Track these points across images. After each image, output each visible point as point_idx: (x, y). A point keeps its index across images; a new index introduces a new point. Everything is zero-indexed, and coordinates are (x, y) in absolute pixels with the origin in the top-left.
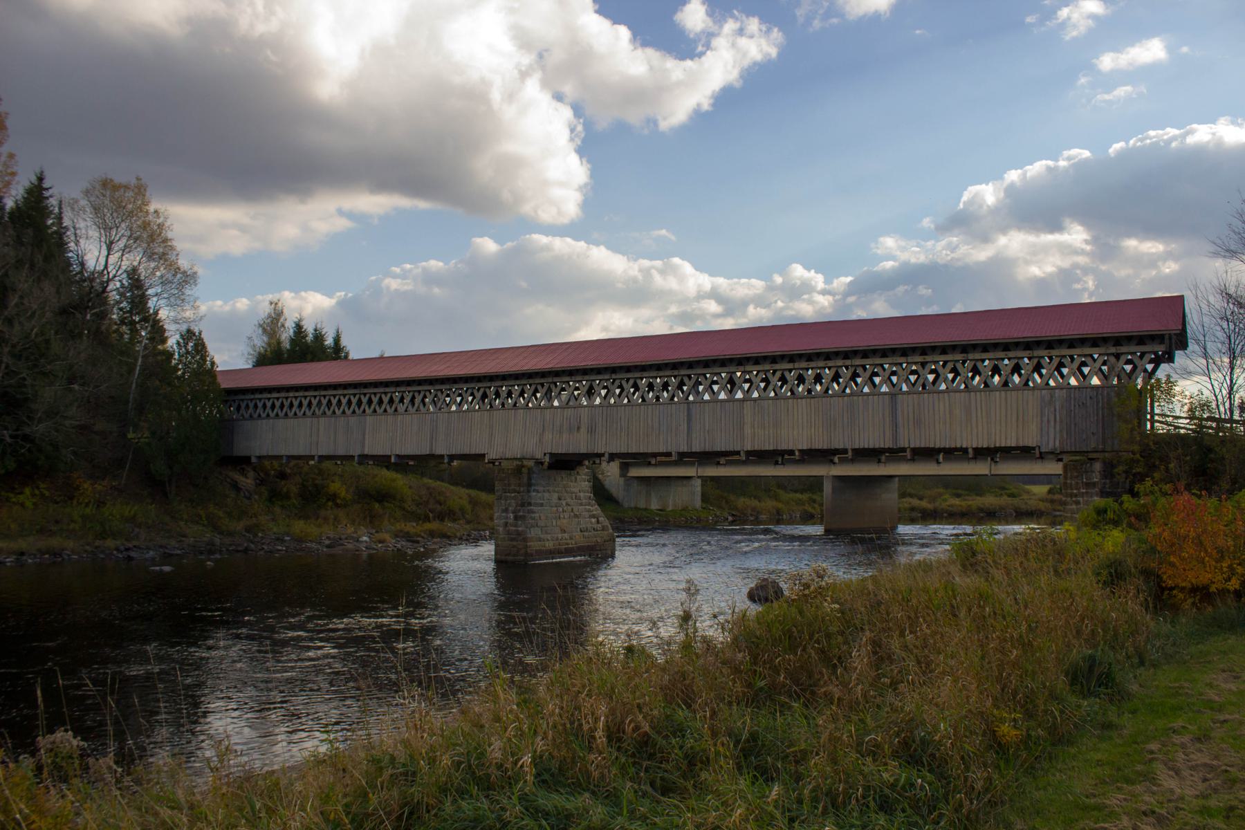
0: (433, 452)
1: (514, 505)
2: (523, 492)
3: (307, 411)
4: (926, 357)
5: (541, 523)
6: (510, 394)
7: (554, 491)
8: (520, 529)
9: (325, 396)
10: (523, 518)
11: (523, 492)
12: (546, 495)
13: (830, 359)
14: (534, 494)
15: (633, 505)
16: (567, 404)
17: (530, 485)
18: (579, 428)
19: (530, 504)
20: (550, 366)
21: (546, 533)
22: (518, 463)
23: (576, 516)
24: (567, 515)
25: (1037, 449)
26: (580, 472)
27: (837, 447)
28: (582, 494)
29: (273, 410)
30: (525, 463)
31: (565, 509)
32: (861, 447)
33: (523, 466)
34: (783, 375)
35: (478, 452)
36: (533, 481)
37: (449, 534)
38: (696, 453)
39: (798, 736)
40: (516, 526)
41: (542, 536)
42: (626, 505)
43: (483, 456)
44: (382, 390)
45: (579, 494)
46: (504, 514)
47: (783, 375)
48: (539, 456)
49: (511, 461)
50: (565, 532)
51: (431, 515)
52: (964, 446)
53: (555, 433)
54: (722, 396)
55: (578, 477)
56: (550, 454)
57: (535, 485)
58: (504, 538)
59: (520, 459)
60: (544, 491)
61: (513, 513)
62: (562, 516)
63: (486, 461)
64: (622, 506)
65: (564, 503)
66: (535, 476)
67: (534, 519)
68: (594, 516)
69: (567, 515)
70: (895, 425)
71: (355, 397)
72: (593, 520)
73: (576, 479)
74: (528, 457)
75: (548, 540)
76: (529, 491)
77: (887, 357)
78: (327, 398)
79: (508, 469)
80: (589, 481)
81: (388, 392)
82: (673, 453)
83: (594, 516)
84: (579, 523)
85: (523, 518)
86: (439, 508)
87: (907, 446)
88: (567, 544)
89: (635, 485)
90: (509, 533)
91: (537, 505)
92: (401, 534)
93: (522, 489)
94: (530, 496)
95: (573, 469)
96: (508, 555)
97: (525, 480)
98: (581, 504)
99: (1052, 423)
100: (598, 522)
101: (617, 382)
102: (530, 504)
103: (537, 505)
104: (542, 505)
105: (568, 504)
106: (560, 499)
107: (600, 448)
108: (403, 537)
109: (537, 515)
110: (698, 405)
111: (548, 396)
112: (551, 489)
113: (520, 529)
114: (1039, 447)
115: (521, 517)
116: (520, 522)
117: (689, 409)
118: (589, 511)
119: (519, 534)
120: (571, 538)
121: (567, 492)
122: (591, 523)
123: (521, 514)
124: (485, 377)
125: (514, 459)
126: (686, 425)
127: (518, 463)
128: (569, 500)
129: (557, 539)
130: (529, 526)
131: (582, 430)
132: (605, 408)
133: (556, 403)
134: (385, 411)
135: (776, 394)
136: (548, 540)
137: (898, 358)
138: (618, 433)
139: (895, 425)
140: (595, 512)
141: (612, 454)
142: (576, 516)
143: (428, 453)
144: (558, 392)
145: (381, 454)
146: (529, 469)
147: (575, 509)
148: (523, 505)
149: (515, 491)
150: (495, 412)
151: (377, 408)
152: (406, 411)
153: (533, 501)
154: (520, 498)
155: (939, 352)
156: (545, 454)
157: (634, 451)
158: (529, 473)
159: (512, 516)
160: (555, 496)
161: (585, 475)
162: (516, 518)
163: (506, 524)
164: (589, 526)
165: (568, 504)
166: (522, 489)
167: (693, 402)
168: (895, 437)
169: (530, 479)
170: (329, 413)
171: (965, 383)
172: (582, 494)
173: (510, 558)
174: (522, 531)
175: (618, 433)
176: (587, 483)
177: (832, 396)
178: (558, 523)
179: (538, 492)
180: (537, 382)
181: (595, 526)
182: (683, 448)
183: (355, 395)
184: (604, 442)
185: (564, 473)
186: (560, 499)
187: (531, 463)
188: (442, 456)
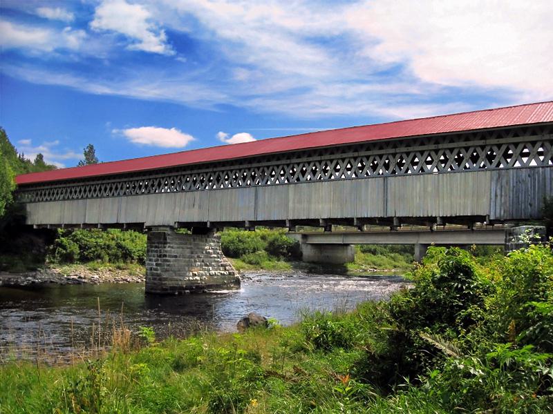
4: (409, 148)
6: (62, 193)
7: (188, 248)
13: (345, 153)
14: (169, 249)
18: (194, 205)
19: (165, 256)
25: (487, 217)
27: (347, 217)
29: (105, 192)
35: (141, 222)
36: (168, 241)
39: (517, 394)
43: (143, 223)
47: (401, 156)
48: (172, 224)
52: (434, 216)
56: (178, 222)
65: (196, 256)
70: (386, 201)
73: (206, 240)
81: (370, 156)
82: (438, 219)
93: (160, 245)
96: (152, 289)
99: (499, 197)
105: (198, 257)
106: (192, 253)
114: (489, 216)
121: (198, 248)
131: (195, 206)
137: (527, 137)
139: (386, 201)
144: (269, 172)
145: (134, 222)
152: (190, 189)
155: (392, 146)
157: (224, 220)
168: (386, 209)
170: (111, 195)
171: (437, 167)
173: (153, 291)
177: (333, 180)
179: (172, 247)
180: (374, 154)
182: (252, 219)
188: (123, 224)
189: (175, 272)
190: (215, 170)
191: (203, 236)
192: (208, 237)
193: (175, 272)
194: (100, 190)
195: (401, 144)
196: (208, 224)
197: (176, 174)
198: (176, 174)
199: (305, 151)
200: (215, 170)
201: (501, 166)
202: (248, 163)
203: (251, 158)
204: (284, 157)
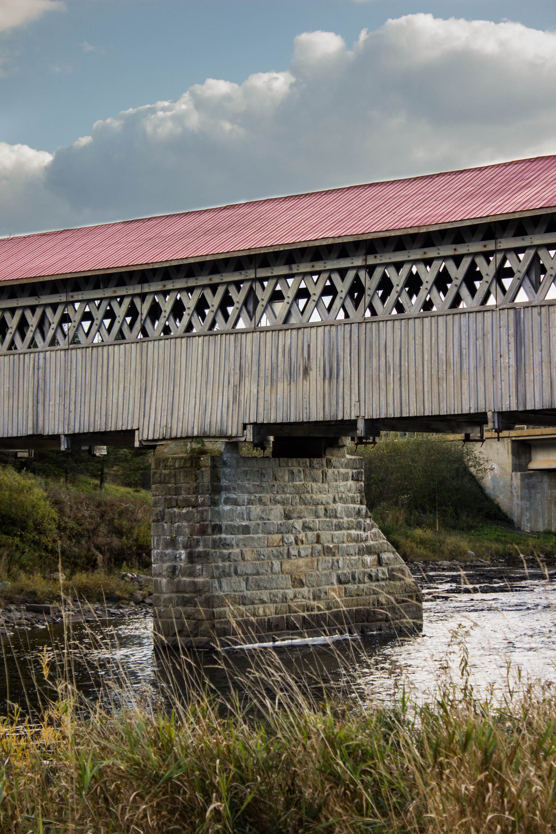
0: (40, 431)
1: (187, 531)
2: (203, 504)
3: (38, 338)
5: (246, 567)
7: (276, 502)
8: (200, 580)
9: (33, 309)
10: (205, 557)
11: (203, 504)
12: (256, 509)
14: (227, 508)
15: (541, 527)
16: (286, 321)
17: (216, 489)
18: (306, 371)
19: (217, 529)
20: (268, 243)
21: (259, 587)
22: (195, 446)
23: (328, 551)
24: (305, 549)
26: (334, 459)
28: (339, 506)
30: (209, 445)
31: (302, 536)
32: (383, 416)
33: (203, 452)
34: (132, 304)
36: (224, 482)
37: (118, 593)
38: (534, 412)
40: (191, 574)
41: (248, 593)
42: (527, 527)
43: (131, 433)
44: (476, 247)
45: (332, 506)
46: (169, 551)
47: (132, 304)
48: (233, 430)
49: (181, 443)
50: (302, 584)
51: (100, 557)
53: (262, 382)
54: (522, 297)
55: (330, 471)
56: (255, 424)
57: (228, 489)
58: (170, 599)
59: (199, 438)
60: (250, 502)
61: (185, 548)
62: (294, 552)
63: (137, 444)
64: (519, 529)
65: (298, 524)
66: (227, 470)
67: (228, 558)
68: (369, 551)
69: (305, 549)
71: (33, 313)
72: (369, 559)
73: (324, 474)
74: (213, 432)
75: (263, 602)
76: (215, 503)
77: (58, 293)
78: (351, 275)
79: (175, 459)
80: (355, 479)
82: (490, 414)
83: (369, 551)
84: (334, 566)
85: (205, 557)
86: (116, 542)
87: (61, 431)
88: (309, 608)
89: (546, 485)
90: (178, 589)
91: (232, 530)
92: (21, 597)
94: (218, 514)
95: (319, 455)
97: (206, 480)
98: (339, 527)
100: (380, 562)
101: (105, 306)
102: (217, 529)
103: (232, 530)
104: (246, 530)
105: (306, 527)
106: (288, 517)
107: (347, 410)
108: (24, 602)
109: (237, 551)
110: (536, 310)
111: (251, 307)
112: (266, 497)
113: (200, 580)
115: (200, 555)
116: (199, 567)
117: (518, 322)
118: (358, 540)
119: (197, 590)
120: (316, 597)
121: (304, 502)
122: (364, 564)
123: (201, 549)
124: (414, 237)
125: (187, 437)
126: (512, 354)
127: (195, 446)
128: (309, 519)
129: (285, 598)
130: (216, 573)
131: (312, 374)
132: (355, 327)
133: (265, 322)
134: (428, 305)
135: (347, 316)
136: (263, 602)
137: (538, 236)
138: (382, 375)
140: (371, 543)
141: (372, 420)
142: (328, 551)
143: (30, 432)
146: (213, 459)
147: (325, 536)
148: (203, 531)
149: (187, 503)
150: (151, 344)
151: (38, 338)
153: (225, 523)
154: (197, 517)
156: (245, 426)
158: (214, 467)
159: (183, 553)
160: (278, 509)
161: (347, 466)
162: (191, 558)
163: (173, 570)
164: (359, 571)
165: (306, 527)
166: (200, 500)
167: (526, 306)
169: (215, 477)
172: (339, 506)
174: (205, 584)
175: (382, 375)
176: (350, 483)
178: (287, 566)
179: (236, 503)
180: (329, 267)
181: (373, 571)
183: (237, 284)
184: (355, 398)
185: (295, 465)
186: (288, 517)
187: (220, 446)
189: (246, 577)
190: (371, 261)
191: (315, 461)
192: (329, 463)
193: (246, 577)
194: (23, 325)
195: (131, 279)
196: (361, 425)
197: (236, 277)
198: (236, 277)
199: (279, 252)
200: (371, 261)
201: (492, 301)
202: (484, 239)
203: (489, 225)
204: (87, 284)
